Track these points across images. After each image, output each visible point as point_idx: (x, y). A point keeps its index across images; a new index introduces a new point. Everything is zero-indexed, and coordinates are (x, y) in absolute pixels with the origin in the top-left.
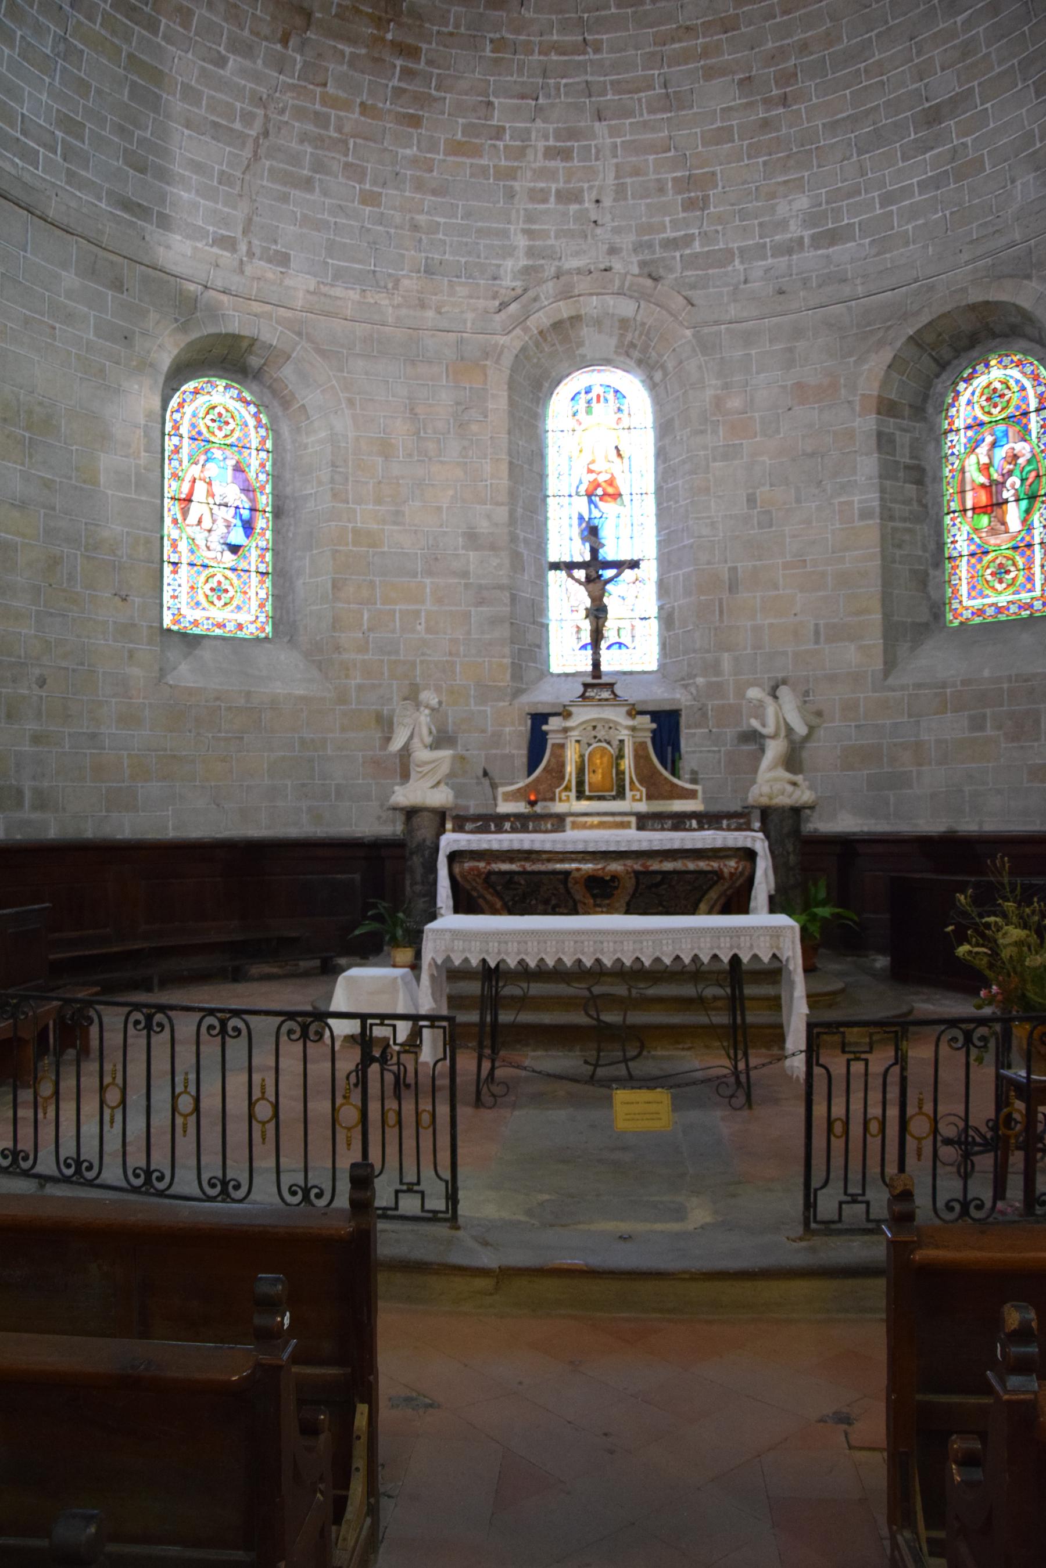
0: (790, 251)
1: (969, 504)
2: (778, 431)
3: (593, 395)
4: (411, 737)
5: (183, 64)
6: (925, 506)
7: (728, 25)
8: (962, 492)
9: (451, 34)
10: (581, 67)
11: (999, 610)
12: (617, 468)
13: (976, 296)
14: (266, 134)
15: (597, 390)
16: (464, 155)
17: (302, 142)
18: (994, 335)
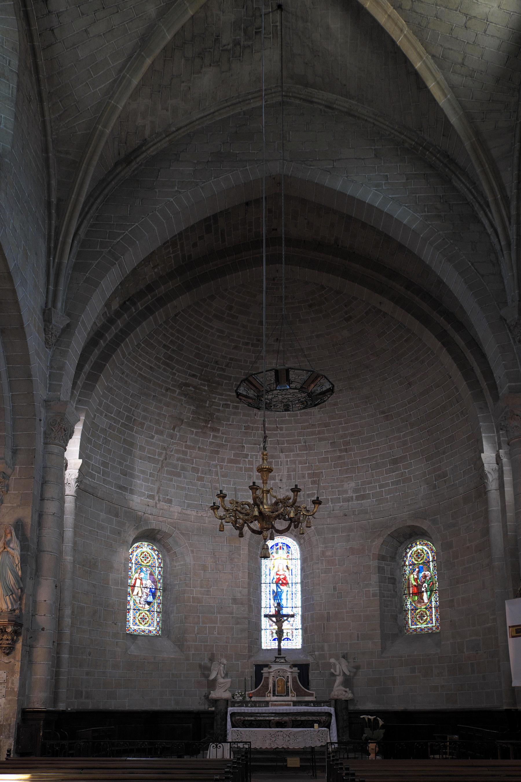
0: (349, 501)
1: (411, 592)
2: (344, 564)
3: (279, 547)
4: (217, 674)
5: (140, 439)
6: (396, 592)
7: (326, 425)
8: (409, 588)
9: (231, 424)
10: (276, 435)
11: (422, 630)
12: (287, 573)
13: (410, 523)
14: (166, 459)
15: (280, 545)
16: (234, 463)
17: (178, 461)
18: (418, 535)
